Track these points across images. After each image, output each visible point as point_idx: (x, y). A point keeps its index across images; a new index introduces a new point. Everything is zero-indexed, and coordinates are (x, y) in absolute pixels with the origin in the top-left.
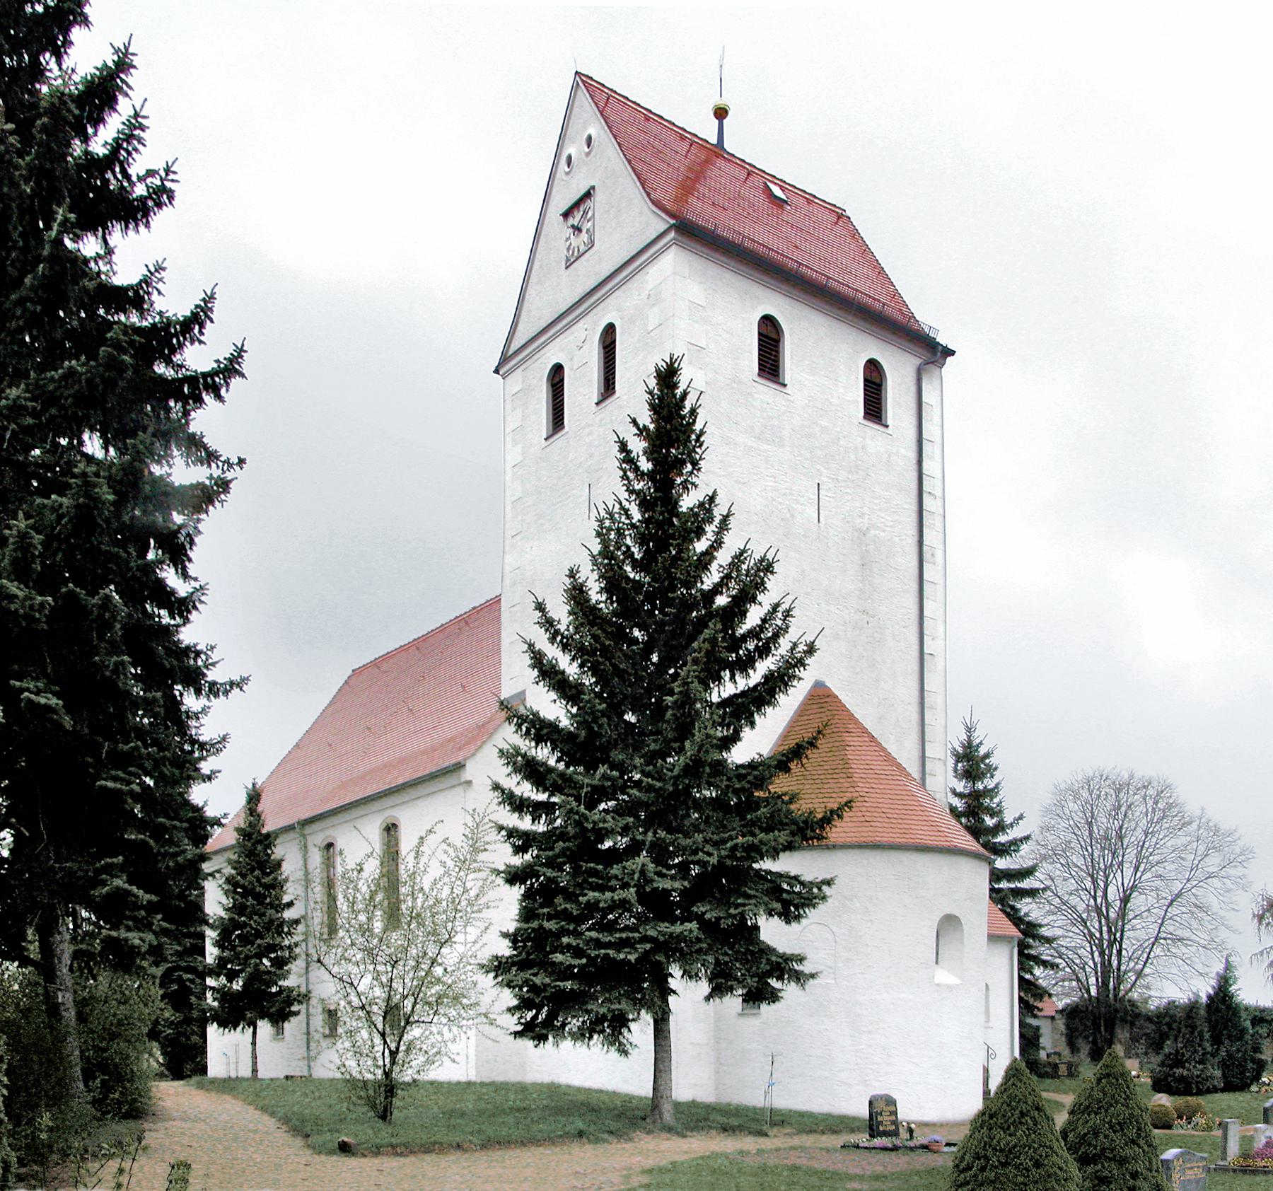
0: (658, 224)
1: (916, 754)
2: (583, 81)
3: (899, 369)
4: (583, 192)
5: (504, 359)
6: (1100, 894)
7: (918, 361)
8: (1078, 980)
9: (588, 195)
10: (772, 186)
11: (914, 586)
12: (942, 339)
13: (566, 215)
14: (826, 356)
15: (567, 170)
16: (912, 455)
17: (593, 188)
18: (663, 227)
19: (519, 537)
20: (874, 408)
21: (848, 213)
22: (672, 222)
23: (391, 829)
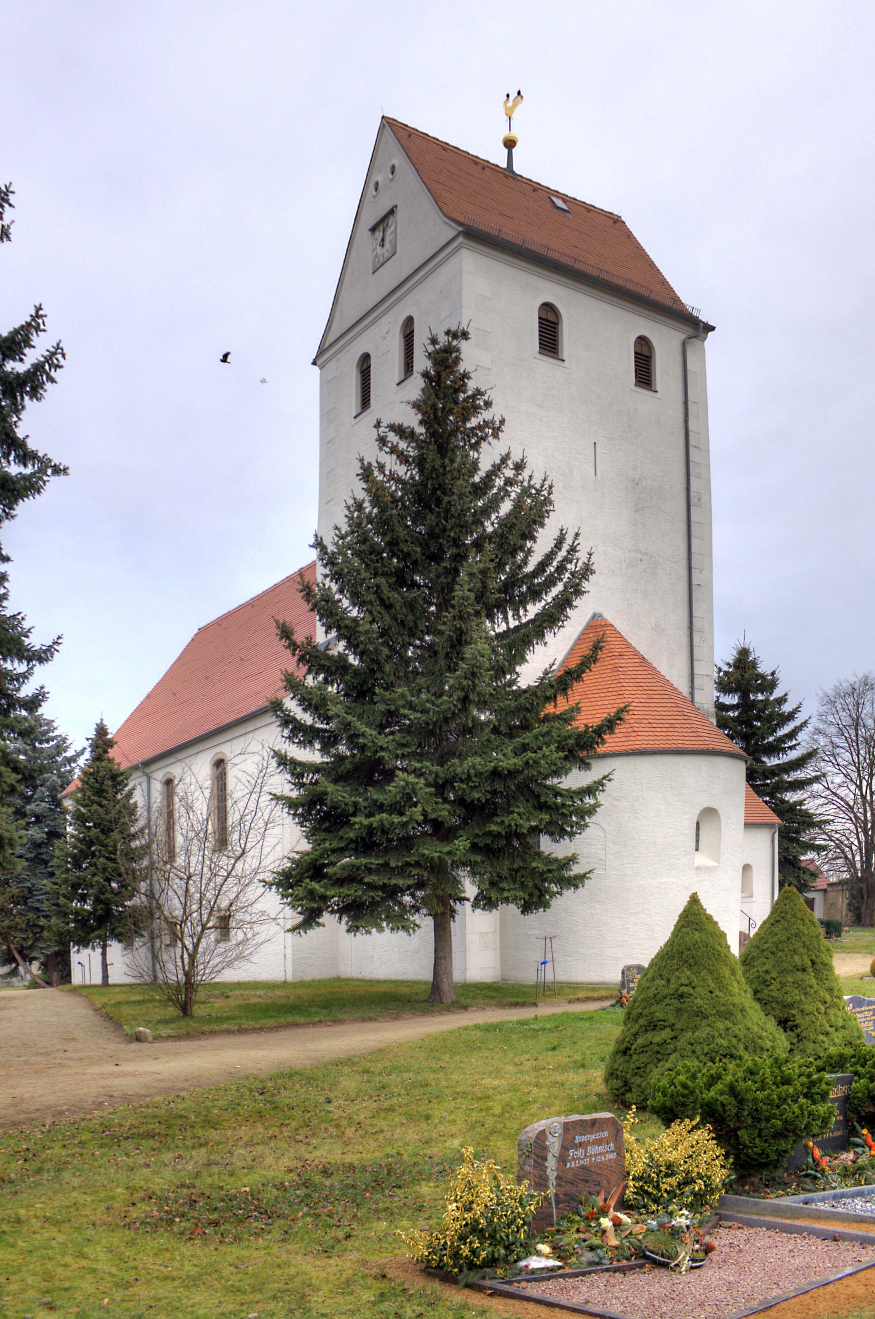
0: (450, 231)
1: (686, 672)
2: (389, 124)
3: (665, 341)
4: (387, 210)
5: (321, 352)
6: (864, 783)
7: (683, 336)
8: (846, 858)
9: (392, 212)
10: (554, 199)
11: (683, 526)
12: (703, 318)
13: (373, 230)
14: (600, 332)
15: (374, 193)
16: (680, 415)
17: (396, 206)
18: (453, 233)
19: (332, 503)
20: (644, 375)
21: (623, 219)
22: (460, 229)
23: (220, 763)
